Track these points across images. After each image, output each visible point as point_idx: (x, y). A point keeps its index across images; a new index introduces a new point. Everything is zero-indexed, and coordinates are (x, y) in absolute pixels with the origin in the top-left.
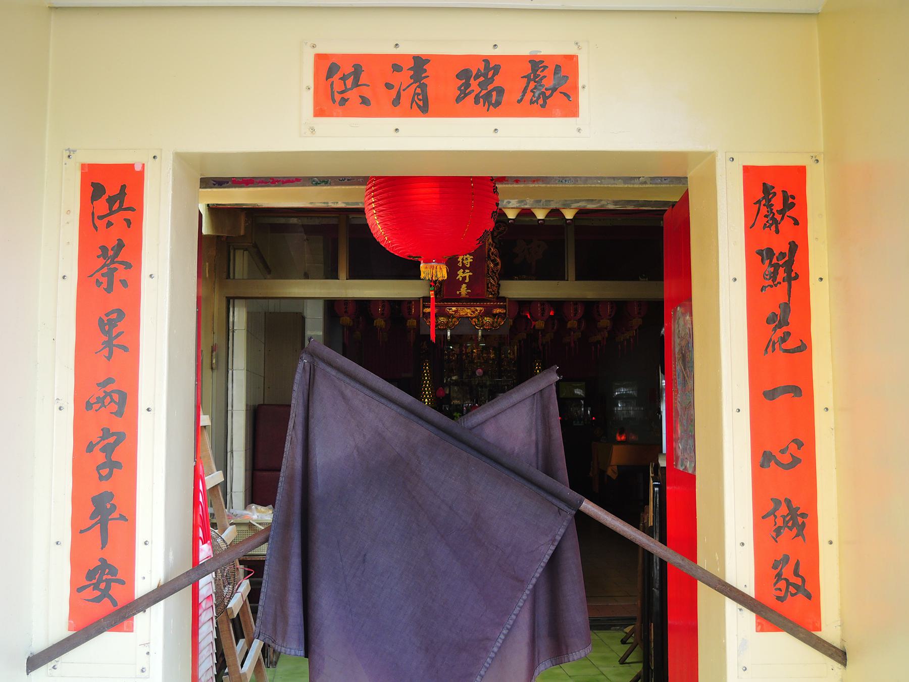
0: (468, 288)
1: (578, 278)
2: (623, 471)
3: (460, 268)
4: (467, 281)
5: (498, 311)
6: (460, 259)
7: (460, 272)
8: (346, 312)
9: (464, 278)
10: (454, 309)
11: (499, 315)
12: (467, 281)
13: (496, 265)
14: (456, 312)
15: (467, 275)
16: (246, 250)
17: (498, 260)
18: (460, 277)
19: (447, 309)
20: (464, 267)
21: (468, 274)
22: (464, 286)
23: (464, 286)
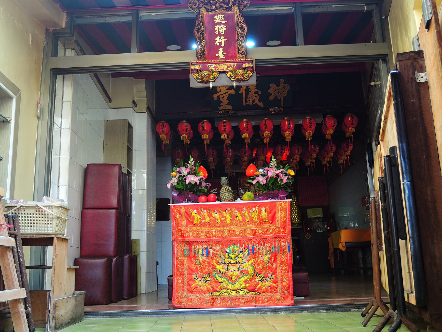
0: (224, 51)
1: (306, 44)
2: (350, 247)
3: (216, 36)
4: (223, 45)
5: (247, 65)
6: (216, 29)
7: (217, 39)
8: (163, 131)
9: (221, 43)
10: (214, 65)
11: (248, 68)
12: (223, 45)
13: (243, 30)
14: (215, 67)
15: (223, 41)
16: (73, 49)
17: (245, 26)
18: (217, 43)
19: (209, 66)
20: (220, 35)
21: (223, 40)
22: (221, 49)
23: (221, 49)
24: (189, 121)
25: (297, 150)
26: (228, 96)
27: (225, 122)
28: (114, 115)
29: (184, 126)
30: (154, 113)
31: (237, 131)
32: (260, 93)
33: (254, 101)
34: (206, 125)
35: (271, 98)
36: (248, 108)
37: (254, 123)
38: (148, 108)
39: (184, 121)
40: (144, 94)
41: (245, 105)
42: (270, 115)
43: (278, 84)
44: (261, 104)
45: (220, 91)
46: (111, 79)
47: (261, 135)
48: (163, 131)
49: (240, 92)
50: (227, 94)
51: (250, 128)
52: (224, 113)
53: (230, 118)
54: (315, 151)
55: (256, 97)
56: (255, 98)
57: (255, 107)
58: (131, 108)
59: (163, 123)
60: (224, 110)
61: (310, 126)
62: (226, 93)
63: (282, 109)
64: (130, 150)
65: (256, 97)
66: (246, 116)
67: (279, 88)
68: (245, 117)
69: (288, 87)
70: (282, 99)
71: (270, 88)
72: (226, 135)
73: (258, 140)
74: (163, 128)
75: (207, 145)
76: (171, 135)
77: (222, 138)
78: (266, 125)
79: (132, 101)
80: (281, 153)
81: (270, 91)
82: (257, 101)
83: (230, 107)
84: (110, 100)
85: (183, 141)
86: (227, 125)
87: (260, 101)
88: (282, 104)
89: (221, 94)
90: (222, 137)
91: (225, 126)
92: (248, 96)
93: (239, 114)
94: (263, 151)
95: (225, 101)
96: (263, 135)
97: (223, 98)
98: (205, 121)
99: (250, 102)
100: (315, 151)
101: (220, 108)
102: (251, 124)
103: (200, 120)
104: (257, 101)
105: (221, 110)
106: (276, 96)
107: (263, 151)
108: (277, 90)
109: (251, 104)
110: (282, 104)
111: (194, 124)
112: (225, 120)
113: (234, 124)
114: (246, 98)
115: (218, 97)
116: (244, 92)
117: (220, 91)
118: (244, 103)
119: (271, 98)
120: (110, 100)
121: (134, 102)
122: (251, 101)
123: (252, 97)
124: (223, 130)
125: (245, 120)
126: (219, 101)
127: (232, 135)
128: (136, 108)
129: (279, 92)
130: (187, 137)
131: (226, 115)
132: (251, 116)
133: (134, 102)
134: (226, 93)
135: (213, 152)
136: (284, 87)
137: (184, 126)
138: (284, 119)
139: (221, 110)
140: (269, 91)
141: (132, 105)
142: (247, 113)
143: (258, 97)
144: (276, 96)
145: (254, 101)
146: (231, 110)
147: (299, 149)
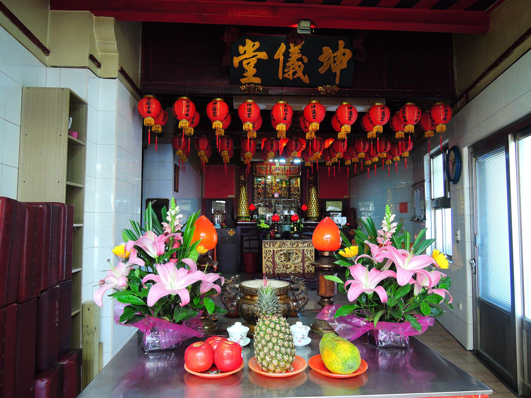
24: (193, 98)
26: (256, 62)
27: (250, 104)
28: (52, 79)
29: (219, 106)
30: (138, 85)
32: (306, 60)
33: (295, 73)
34: (219, 106)
35: (322, 70)
36: (285, 83)
37: (262, 107)
38: (122, 71)
39: (185, 98)
40: (113, 45)
41: (281, 78)
42: (317, 95)
43: (335, 49)
44: (306, 79)
45: (245, 53)
46: (50, 12)
48: (149, 112)
49: (276, 57)
50: (255, 59)
52: (249, 89)
53: (258, 96)
54: (364, 150)
55: (299, 66)
56: (297, 69)
57: (296, 83)
58: (85, 68)
59: (149, 99)
60: (248, 84)
62: (253, 57)
63: (336, 88)
64: (75, 149)
65: (299, 66)
67: (335, 54)
68: (281, 97)
70: (338, 73)
72: (251, 125)
74: (149, 108)
75: (221, 137)
76: (164, 118)
78: (314, 112)
79: (88, 56)
81: (321, 58)
82: (300, 74)
83: (258, 80)
84: (46, 51)
85: (182, 129)
86: (253, 108)
87: (304, 73)
89: (246, 59)
91: (314, 112)
92: (288, 64)
93: (271, 92)
94: (296, 145)
95: (251, 70)
97: (248, 64)
98: (219, 99)
99: (289, 75)
100: (364, 150)
101: (243, 81)
103: (210, 98)
104: (300, 74)
105: (244, 84)
109: (291, 77)
111: (201, 103)
112: (250, 101)
114: (284, 67)
115: (241, 63)
116: (282, 58)
117: (245, 53)
118: (280, 76)
119: (322, 70)
120: (46, 51)
121: (92, 58)
122: (291, 72)
123: (293, 67)
124: (246, 115)
125: (281, 102)
126: (241, 70)
128: (99, 71)
129: (335, 62)
130: (188, 124)
132: (288, 96)
133: (92, 58)
134: (253, 57)
136: (344, 54)
137: (184, 106)
138: (341, 104)
139: (244, 84)
140: (319, 58)
141: (87, 62)
146: (259, 84)
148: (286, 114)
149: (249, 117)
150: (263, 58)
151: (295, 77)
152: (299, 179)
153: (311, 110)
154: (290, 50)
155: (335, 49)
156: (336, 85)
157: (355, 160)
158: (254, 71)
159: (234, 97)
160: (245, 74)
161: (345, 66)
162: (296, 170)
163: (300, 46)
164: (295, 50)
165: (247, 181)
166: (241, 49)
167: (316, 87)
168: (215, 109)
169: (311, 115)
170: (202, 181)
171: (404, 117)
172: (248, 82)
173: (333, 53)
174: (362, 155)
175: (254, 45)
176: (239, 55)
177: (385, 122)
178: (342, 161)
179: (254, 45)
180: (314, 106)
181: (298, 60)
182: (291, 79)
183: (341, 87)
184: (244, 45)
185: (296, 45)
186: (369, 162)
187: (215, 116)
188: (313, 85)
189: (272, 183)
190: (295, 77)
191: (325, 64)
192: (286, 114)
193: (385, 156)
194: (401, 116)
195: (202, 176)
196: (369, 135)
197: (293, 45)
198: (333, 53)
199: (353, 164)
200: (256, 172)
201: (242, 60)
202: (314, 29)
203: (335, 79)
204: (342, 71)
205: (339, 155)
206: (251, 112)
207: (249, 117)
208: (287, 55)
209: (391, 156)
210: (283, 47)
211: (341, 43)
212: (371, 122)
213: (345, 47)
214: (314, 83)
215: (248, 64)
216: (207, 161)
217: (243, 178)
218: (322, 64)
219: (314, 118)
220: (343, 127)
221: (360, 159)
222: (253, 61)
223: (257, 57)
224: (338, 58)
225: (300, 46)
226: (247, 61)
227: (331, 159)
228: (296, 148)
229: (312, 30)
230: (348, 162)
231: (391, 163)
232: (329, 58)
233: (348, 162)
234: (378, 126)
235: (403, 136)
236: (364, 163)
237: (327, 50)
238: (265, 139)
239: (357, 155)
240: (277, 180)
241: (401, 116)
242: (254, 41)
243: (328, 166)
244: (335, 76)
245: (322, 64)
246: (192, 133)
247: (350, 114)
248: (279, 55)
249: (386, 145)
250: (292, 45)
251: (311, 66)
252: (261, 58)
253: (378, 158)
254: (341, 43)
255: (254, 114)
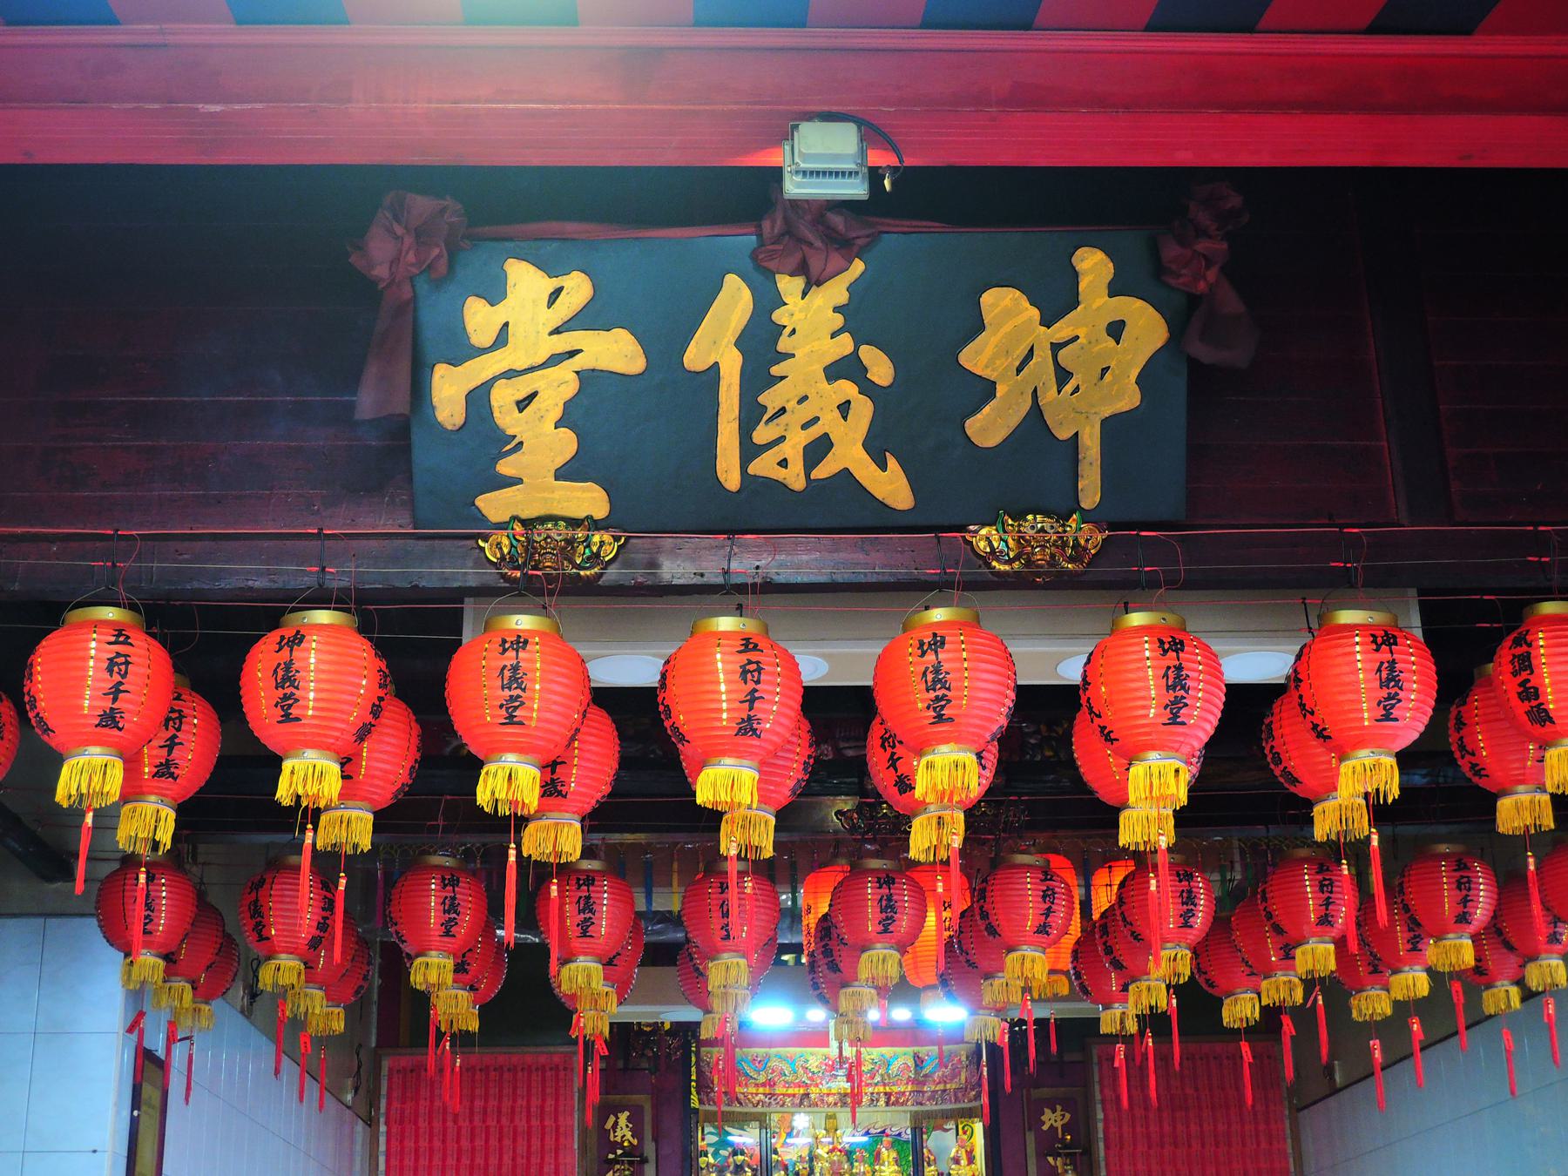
25: (1173, 910)
26: (571, 388)
27: (521, 642)
29: (323, 665)
31: (643, 728)
32: (881, 369)
33: (818, 449)
35: (989, 427)
36: (762, 511)
37: (815, 668)
39: (110, 613)
42: (976, 582)
43: (1056, 299)
44: (891, 486)
47: (881, 777)
49: (695, 358)
51: (777, 712)
55: (844, 408)
56: (830, 422)
57: (835, 508)
61: (1175, 711)
62: (555, 360)
66: (741, 589)
67: (1061, 330)
68: (732, 594)
69: (1148, 328)
71: (977, 326)
73: (846, 803)
77: (483, 797)
78: (937, 679)
80: (1043, 929)
81: (977, 357)
82: (850, 454)
83: (589, 500)
86: (534, 661)
87: (877, 448)
88: (1090, 491)
89: (510, 374)
90: (490, 790)
92: (771, 399)
93: (674, 570)
94: (888, 907)
95: (542, 441)
96: (905, 785)
97: (522, 404)
100: (1325, 920)
101: (494, 505)
102: (792, 666)
103: (267, 614)
104: (850, 454)
105: (502, 526)
106: (1036, 411)
107: (888, 907)
108: (1043, 356)
109: (794, 477)
110: (1090, 491)
111: (209, 644)
113: (629, 667)
114: (751, 414)
115: (478, 398)
116: (731, 365)
118: (729, 474)
119: (989, 427)
122: (797, 441)
124: (491, 715)
126: (484, 440)
127: (594, 769)
129: (1063, 376)
131: (548, 576)
134: (555, 360)
135: (451, 907)
136: (1116, 330)
137: (323, 665)
138: (1115, 630)
142: (750, 560)
143: (863, 409)
144: (1036, 411)
145: (818, 449)
146: (595, 525)
147: (1189, 899)
148: (752, 699)
149: (511, 720)
150: (620, 366)
151: (821, 472)
152: (978, 1127)
153: (916, 664)
154: (779, 316)
155: (1056, 299)
156: (1087, 517)
157: (1283, 988)
158: (565, 444)
159: (469, 606)
160: (505, 467)
161: (1129, 398)
162: (955, 1074)
163: (836, 291)
164: (812, 317)
165: (649, 1150)
166: (480, 319)
167: (962, 528)
168: (287, 677)
169: (921, 699)
170: (373, 1158)
171: (1530, 693)
172: (525, 515)
173: (1047, 322)
174: (1318, 955)
175: (557, 292)
176: (461, 352)
177: (1411, 723)
178: (1197, 999)
179: (557, 292)
180: (938, 643)
181: (834, 372)
182: (798, 484)
183: (1112, 526)
184: (495, 293)
185: (814, 282)
186: (1373, 1004)
187: (287, 718)
188: (933, 521)
189: (812, 1158)
190: (821, 472)
191: (1001, 390)
192: (752, 699)
193: (1468, 957)
194: (1509, 685)
195: (371, 1122)
196: (1324, 825)
197: (799, 283)
198: (1047, 322)
199: (1271, 1014)
200: (704, 1087)
201: (487, 386)
202: (895, 170)
203: (1076, 476)
204: (1113, 427)
205: (1172, 962)
206: (527, 693)
207: (511, 720)
208: (762, 346)
209: (1513, 960)
210: (734, 301)
211: (1093, 266)
212: (1321, 734)
213: (1115, 290)
214: (952, 502)
215: (522, 404)
216: (474, 1025)
217: (623, 1131)
218: (986, 390)
219: (940, 718)
220: (1137, 771)
221: (1310, 984)
222: (558, 386)
223: (578, 362)
224: (1076, 351)
225: (836, 291)
226: (521, 388)
227: (1125, 988)
228: (886, 927)
229: (875, 176)
230: (1241, 1009)
231: (1516, 1002)
232: (1021, 351)
233: (1241, 1009)
234: (1364, 757)
235: (1549, 822)
236: (1474, 1000)
237: (1008, 310)
238: (832, 877)
239: (1288, 956)
240: (850, 1137)
241: (1509, 685)
242: (550, 268)
243: (1112, 1039)
244: (1076, 461)
245: (986, 390)
246: (165, 836)
247: (1176, 681)
248: (715, 346)
249: (1464, 885)
250: (789, 286)
251: (922, 407)
252: (604, 364)
253: (1430, 971)
254: (1093, 266)
255: (545, 699)
